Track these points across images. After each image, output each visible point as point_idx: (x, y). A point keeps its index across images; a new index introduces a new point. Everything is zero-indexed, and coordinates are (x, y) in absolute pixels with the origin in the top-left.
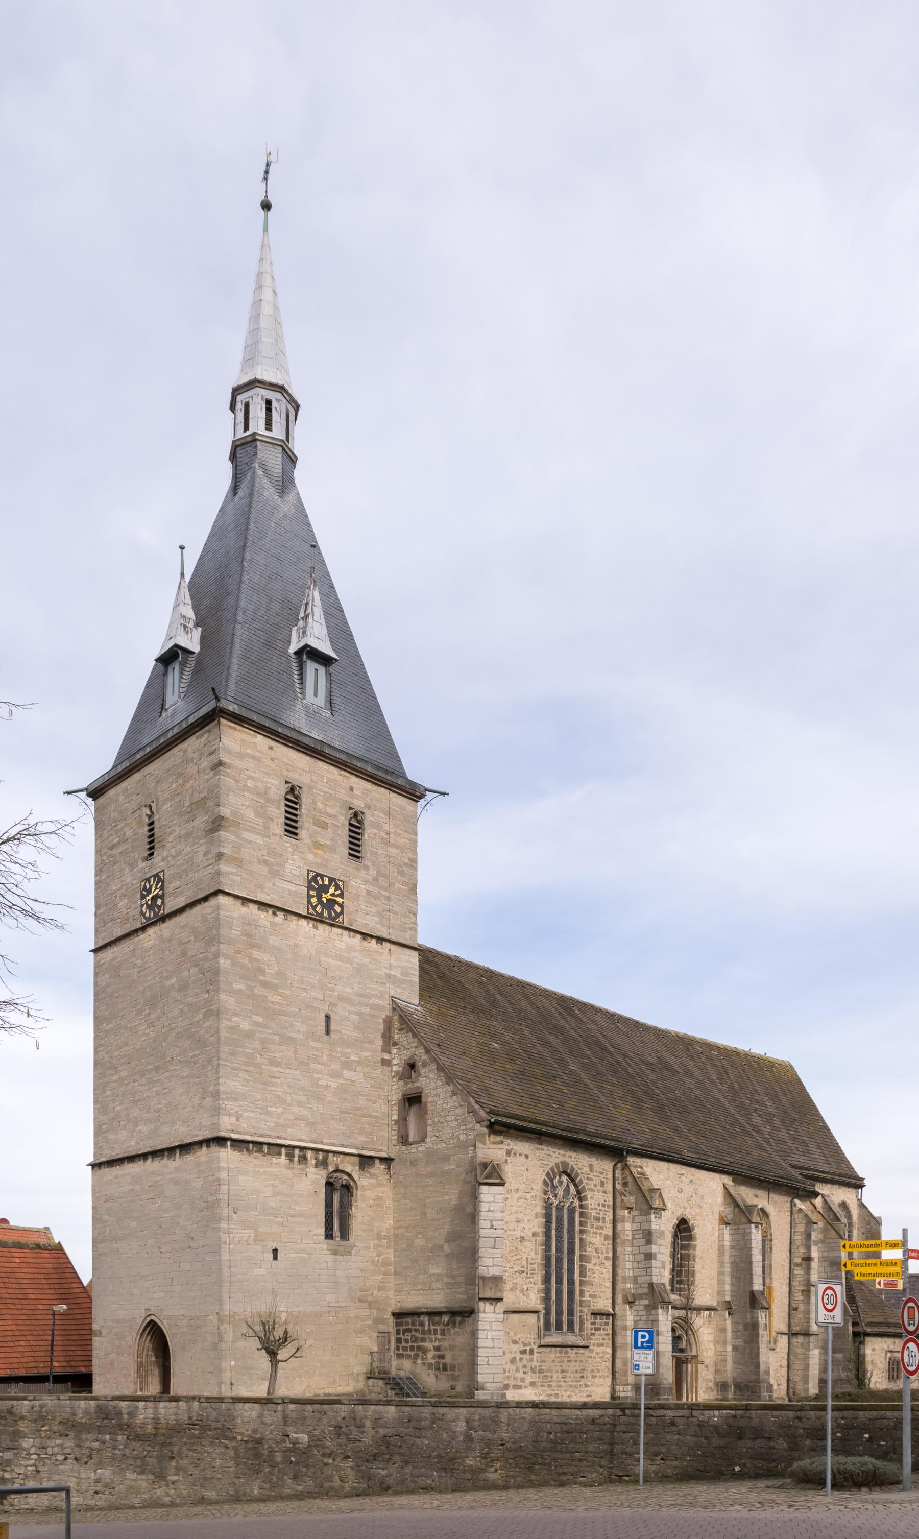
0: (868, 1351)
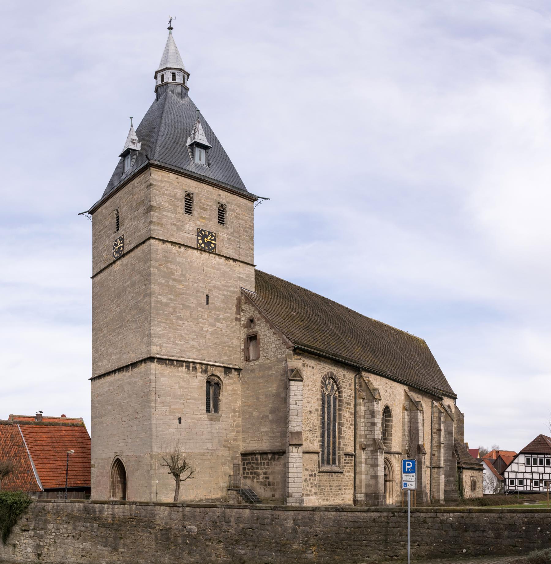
0: (464, 477)
